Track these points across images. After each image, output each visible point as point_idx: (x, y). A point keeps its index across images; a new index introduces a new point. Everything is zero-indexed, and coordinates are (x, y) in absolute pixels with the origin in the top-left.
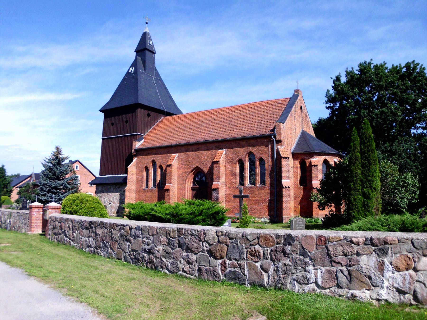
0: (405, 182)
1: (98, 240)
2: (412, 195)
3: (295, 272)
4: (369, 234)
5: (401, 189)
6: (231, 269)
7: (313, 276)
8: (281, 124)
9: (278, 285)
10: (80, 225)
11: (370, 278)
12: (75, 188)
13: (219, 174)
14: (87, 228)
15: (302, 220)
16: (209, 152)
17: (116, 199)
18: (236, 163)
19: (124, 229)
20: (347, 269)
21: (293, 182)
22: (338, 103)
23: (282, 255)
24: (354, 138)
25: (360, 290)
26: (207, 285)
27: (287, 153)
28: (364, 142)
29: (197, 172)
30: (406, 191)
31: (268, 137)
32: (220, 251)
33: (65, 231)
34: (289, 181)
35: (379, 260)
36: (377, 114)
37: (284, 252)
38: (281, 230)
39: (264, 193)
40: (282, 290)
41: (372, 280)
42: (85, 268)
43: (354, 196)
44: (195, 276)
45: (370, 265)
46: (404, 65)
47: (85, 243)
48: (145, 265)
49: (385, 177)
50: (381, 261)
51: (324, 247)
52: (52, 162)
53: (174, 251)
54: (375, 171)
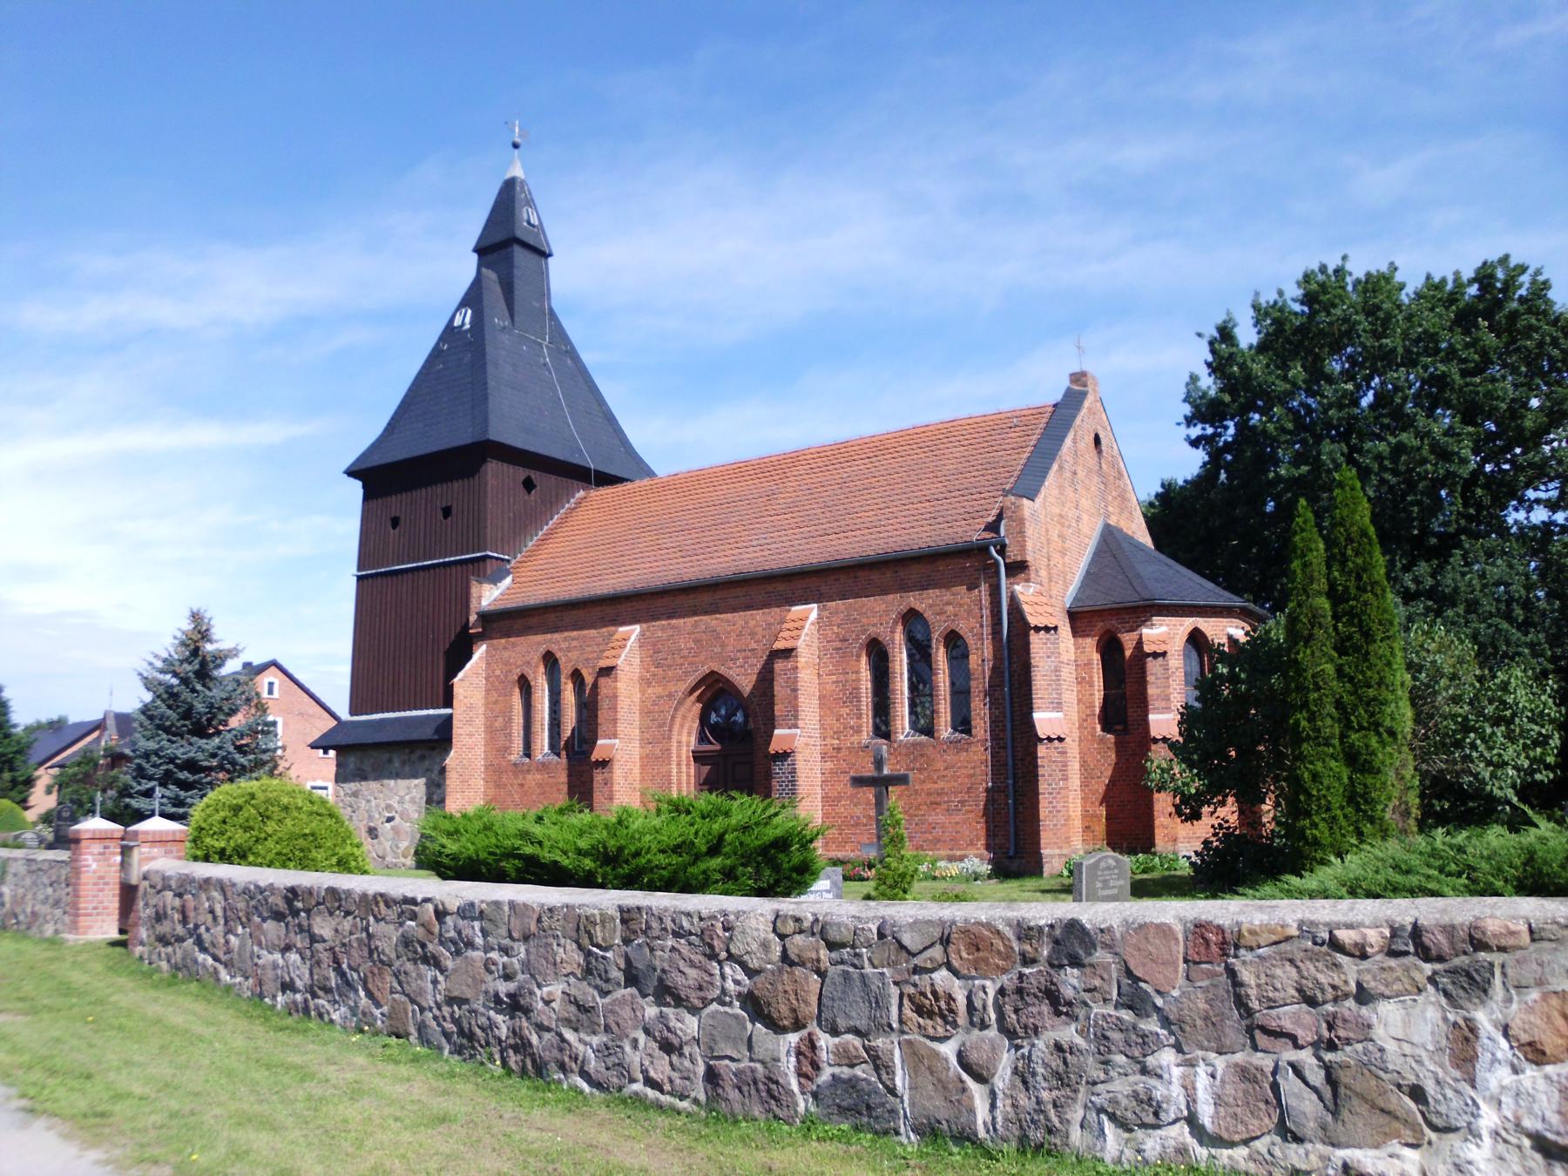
0: (1503, 703)
1: (318, 963)
2: (1532, 754)
3: (1102, 1076)
4: (1405, 911)
5: (1489, 730)
6: (837, 1070)
7: (1177, 1092)
8: (1025, 501)
9: (1031, 1134)
10: (253, 903)
11: (1417, 1094)
12: (264, 763)
13: (796, 698)
14: (278, 916)
15: (1117, 861)
16: (758, 618)
17: (413, 801)
18: (859, 656)
19: (414, 917)
20: (1319, 1059)
21: (1075, 717)
22: (1231, 424)
23: (1046, 1008)
24: (1302, 539)
25: (1377, 1147)
26: (742, 1140)
27: (1050, 610)
28: (1343, 554)
29: (714, 691)
30: (1510, 737)
31: (978, 552)
32: (792, 997)
33: (197, 927)
34: (1060, 715)
35: (1451, 1017)
36: (1379, 457)
37: (1052, 996)
38: (1040, 906)
39: (969, 765)
40: (1049, 1153)
41: (1426, 1103)
42: (259, 1075)
43: (1312, 763)
44: (696, 1101)
45: (1416, 1039)
46: (1473, 275)
47: (270, 974)
48: (497, 1056)
49: (1428, 686)
50: (1462, 1023)
51: (1221, 969)
52: (178, 669)
53: (607, 1000)
54: (1389, 664)
